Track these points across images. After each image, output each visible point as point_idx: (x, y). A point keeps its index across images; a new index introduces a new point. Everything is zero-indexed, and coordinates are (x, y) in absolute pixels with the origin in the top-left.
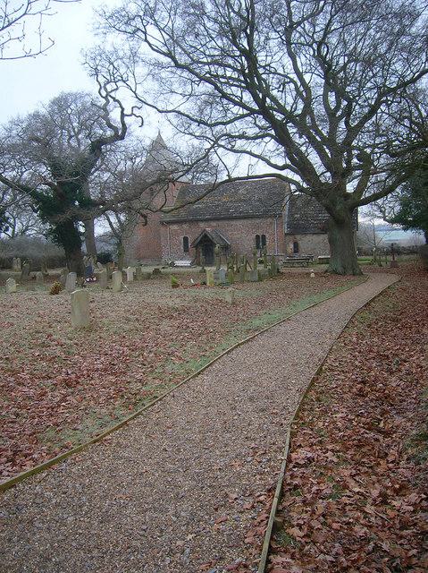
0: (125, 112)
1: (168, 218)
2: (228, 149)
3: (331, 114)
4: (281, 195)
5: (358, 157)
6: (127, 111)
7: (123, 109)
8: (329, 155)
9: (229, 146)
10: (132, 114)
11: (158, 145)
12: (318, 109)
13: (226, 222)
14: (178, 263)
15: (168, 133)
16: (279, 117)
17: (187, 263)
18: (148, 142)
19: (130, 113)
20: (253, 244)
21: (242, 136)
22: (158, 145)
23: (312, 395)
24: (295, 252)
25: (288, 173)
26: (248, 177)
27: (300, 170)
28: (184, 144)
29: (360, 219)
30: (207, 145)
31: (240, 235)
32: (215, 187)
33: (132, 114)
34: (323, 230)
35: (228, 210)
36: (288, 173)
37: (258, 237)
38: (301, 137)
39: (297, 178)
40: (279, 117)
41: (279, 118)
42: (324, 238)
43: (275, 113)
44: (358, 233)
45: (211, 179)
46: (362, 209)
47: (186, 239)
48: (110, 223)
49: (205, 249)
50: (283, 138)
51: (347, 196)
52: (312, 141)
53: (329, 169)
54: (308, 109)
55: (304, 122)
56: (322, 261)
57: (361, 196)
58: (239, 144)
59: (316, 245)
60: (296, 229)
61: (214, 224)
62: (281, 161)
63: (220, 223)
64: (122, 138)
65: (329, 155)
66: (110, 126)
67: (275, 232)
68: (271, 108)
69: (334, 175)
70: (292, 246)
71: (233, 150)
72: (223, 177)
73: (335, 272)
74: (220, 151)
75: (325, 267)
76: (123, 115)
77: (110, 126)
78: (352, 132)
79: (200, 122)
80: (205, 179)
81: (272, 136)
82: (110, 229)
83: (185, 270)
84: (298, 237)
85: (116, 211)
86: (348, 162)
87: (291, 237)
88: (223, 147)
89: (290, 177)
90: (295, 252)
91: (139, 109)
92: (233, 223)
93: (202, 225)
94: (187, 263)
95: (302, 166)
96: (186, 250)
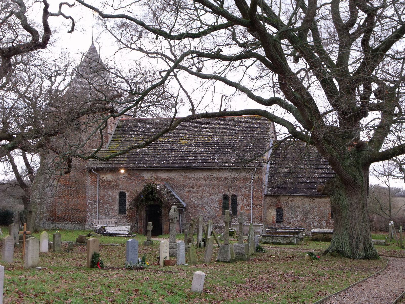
0: (50, 10)
1: (95, 165)
2: (192, 73)
3: (343, 29)
4: (261, 144)
5: (378, 94)
6: (53, 9)
7: (47, 6)
8: (338, 88)
9: (194, 70)
10: (60, 13)
11: (93, 64)
12: (325, 27)
13: (180, 174)
14: (111, 229)
15: (109, 52)
16: (271, 30)
17: (124, 230)
18: (77, 60)
19: (56, 11)
20: (218, 206)
21: (216, 55)
22: (93, 64)
23: (134, 46)
24: (278, 222)
25: (277, 111)
26: (222, 114)
27: (301, 109)
28: (126, 62)
29: (373, 181)
30: (163, 65)
31: (201, 192)
32: (173, 125)
33: (60, 13)
34: (325, 193)
35: (184, 157)
36: (277, 111)
37: (225, 198)
38: (296, 61)
39: (291, 118)
40: (271, 30)
41: (270, 33)
42: (325, 204)
43: (267, 25)
44: (369, 200)
45: (160, 113)
46: (376, 167)
47: (122, 195)
48: (14, 167)
49: (151, 213)
50: (276, 63)
51: (361, 146)
52: (314, 66)
53: (335, 105)
54: (310, 23)
55: (301, 37)
56: (316, 238)
57: (379, 147)
58: (210, 66)
59: (311, 213)
60: (281, 190)
61: (164, 175)
62: (267, 95)
63: (173, 174)
64: (43, 45)
65: (338, 88)
66: (27, 27)
67: (252, 190)
68: (261, 17)
69: (343, 115)
70: (274, 213)
71: (199, 74)
72: (184, 112)
73: (338, 253)
74: (182, 74)
75: (326, 246)
76: (46, 13)
77: (27, 27)
78: (374, 56)
79: (158, 33)
80: (275, 218)
81: (259, 57)
82: (14, 177)
83: (123, 240)
84: (284, 200)
85: (25, 149)
86: (365, 98)
87: (274, 199)
88: (186, 69)
89: (276, 114)
90: (278, 222)
91: (70, 6)
92: (192, 175)
93: (147, 176)
94: (124, 230)
95: (302, 104)
96: (122, 210)
